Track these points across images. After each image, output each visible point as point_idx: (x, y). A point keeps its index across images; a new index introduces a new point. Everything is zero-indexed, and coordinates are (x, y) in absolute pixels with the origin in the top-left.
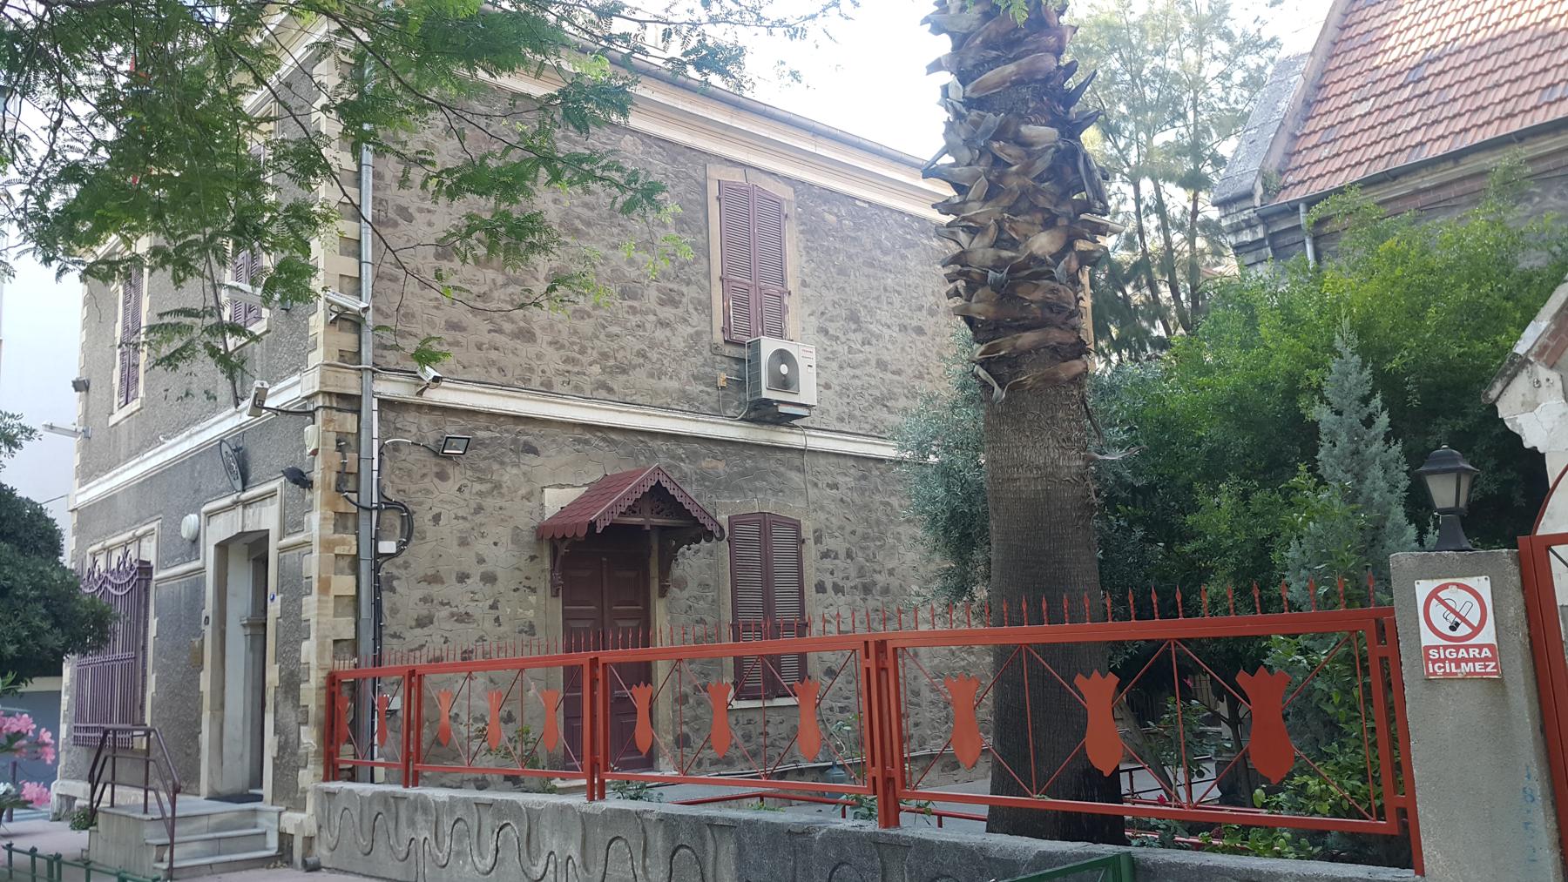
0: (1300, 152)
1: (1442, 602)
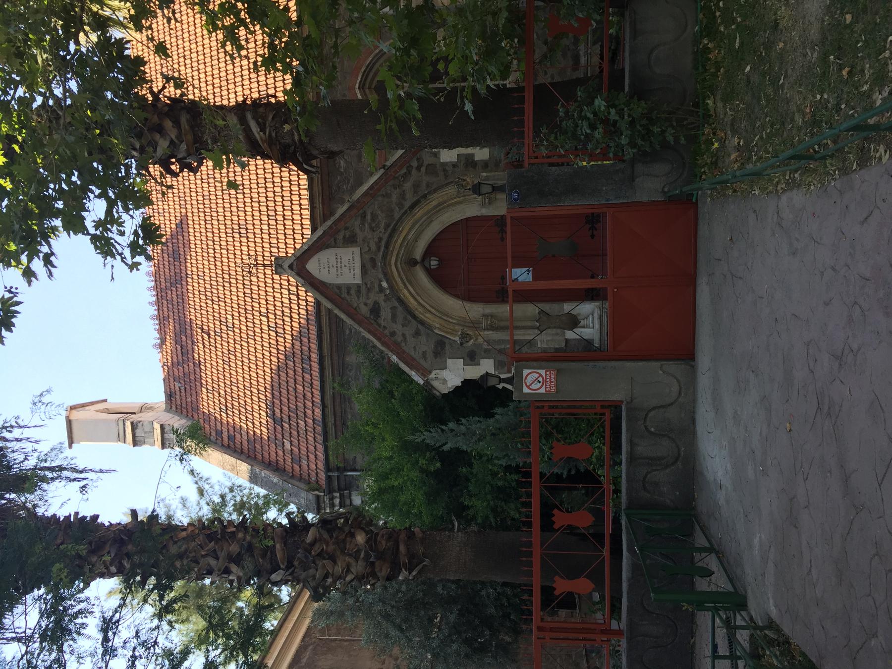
0: (301, 474)
1: (531, 385)
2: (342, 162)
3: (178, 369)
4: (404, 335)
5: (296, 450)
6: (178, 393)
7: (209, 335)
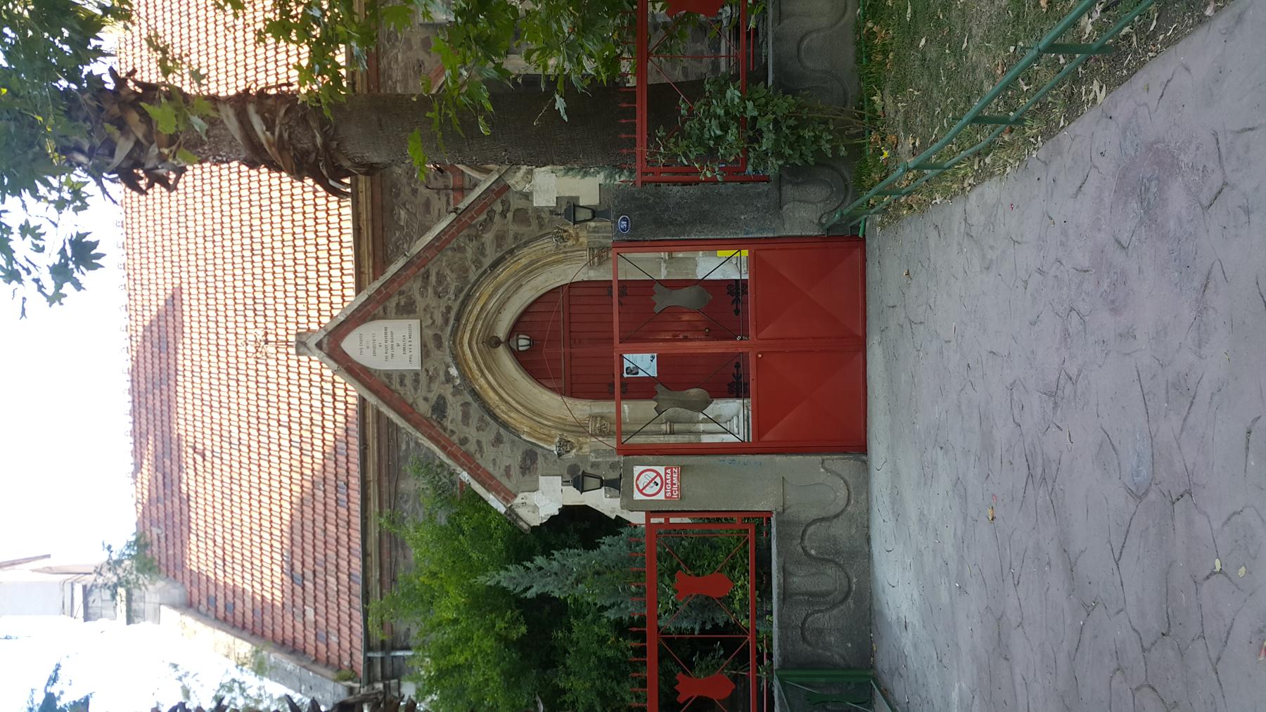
1: (644, 488)
2: (402, 212)
3: (158, 508)
4: (479, 443)
5: (322, 621)
6: (155, 543)
7: (204, 456)
